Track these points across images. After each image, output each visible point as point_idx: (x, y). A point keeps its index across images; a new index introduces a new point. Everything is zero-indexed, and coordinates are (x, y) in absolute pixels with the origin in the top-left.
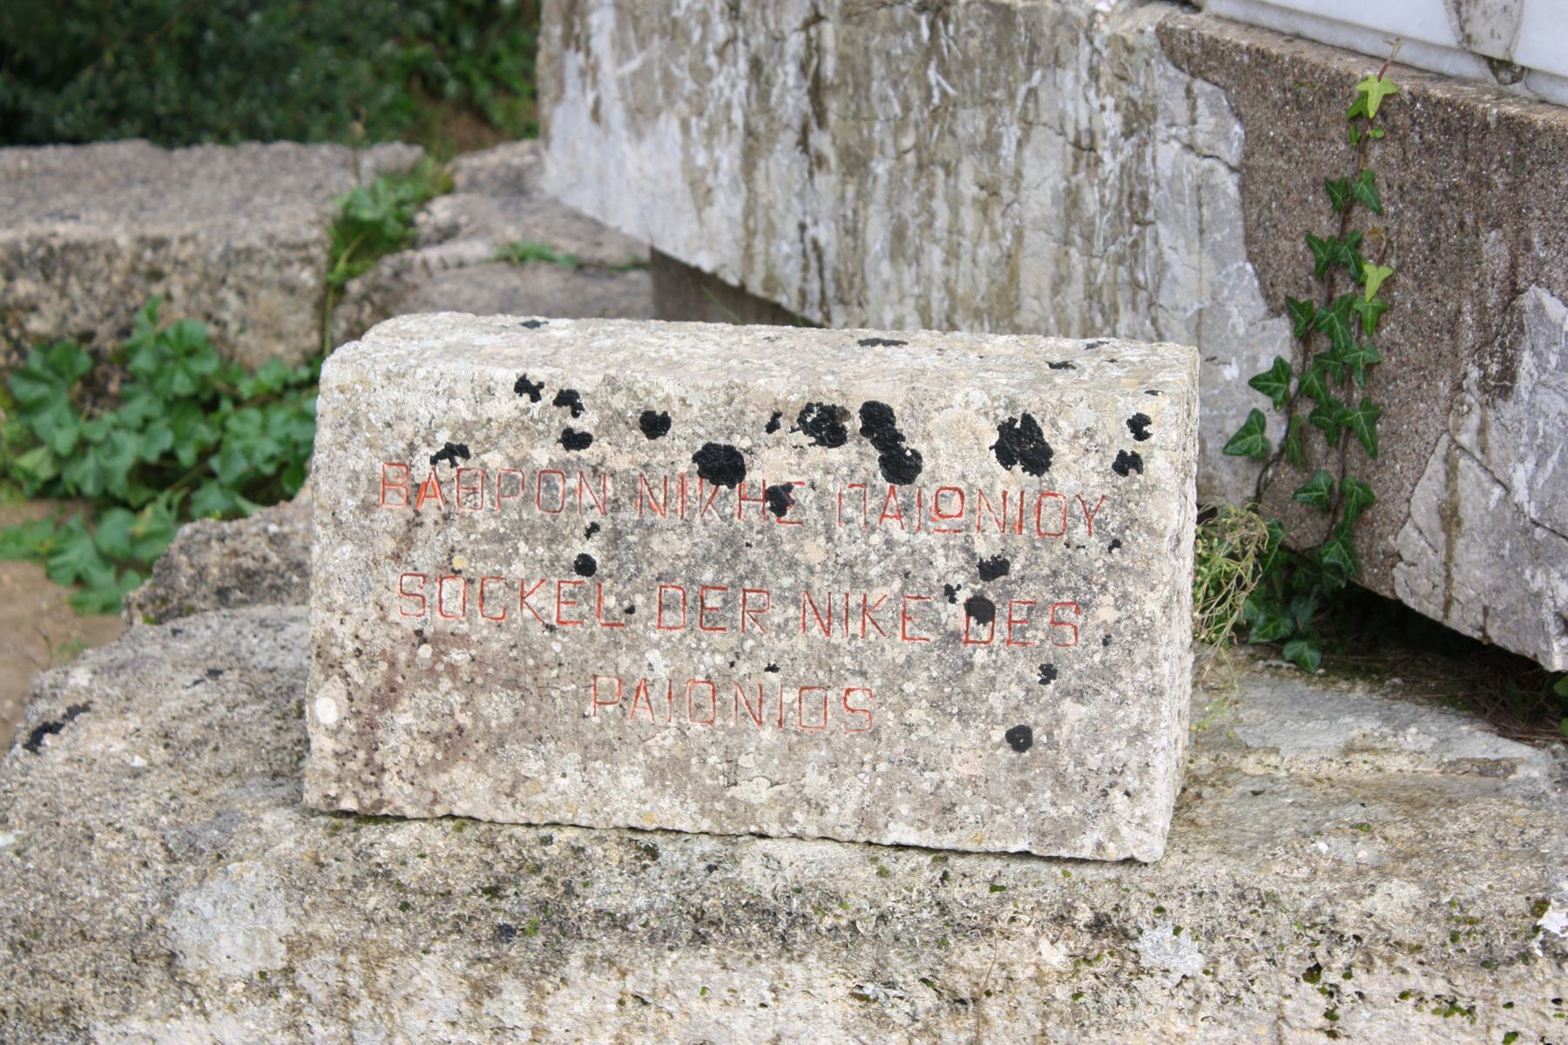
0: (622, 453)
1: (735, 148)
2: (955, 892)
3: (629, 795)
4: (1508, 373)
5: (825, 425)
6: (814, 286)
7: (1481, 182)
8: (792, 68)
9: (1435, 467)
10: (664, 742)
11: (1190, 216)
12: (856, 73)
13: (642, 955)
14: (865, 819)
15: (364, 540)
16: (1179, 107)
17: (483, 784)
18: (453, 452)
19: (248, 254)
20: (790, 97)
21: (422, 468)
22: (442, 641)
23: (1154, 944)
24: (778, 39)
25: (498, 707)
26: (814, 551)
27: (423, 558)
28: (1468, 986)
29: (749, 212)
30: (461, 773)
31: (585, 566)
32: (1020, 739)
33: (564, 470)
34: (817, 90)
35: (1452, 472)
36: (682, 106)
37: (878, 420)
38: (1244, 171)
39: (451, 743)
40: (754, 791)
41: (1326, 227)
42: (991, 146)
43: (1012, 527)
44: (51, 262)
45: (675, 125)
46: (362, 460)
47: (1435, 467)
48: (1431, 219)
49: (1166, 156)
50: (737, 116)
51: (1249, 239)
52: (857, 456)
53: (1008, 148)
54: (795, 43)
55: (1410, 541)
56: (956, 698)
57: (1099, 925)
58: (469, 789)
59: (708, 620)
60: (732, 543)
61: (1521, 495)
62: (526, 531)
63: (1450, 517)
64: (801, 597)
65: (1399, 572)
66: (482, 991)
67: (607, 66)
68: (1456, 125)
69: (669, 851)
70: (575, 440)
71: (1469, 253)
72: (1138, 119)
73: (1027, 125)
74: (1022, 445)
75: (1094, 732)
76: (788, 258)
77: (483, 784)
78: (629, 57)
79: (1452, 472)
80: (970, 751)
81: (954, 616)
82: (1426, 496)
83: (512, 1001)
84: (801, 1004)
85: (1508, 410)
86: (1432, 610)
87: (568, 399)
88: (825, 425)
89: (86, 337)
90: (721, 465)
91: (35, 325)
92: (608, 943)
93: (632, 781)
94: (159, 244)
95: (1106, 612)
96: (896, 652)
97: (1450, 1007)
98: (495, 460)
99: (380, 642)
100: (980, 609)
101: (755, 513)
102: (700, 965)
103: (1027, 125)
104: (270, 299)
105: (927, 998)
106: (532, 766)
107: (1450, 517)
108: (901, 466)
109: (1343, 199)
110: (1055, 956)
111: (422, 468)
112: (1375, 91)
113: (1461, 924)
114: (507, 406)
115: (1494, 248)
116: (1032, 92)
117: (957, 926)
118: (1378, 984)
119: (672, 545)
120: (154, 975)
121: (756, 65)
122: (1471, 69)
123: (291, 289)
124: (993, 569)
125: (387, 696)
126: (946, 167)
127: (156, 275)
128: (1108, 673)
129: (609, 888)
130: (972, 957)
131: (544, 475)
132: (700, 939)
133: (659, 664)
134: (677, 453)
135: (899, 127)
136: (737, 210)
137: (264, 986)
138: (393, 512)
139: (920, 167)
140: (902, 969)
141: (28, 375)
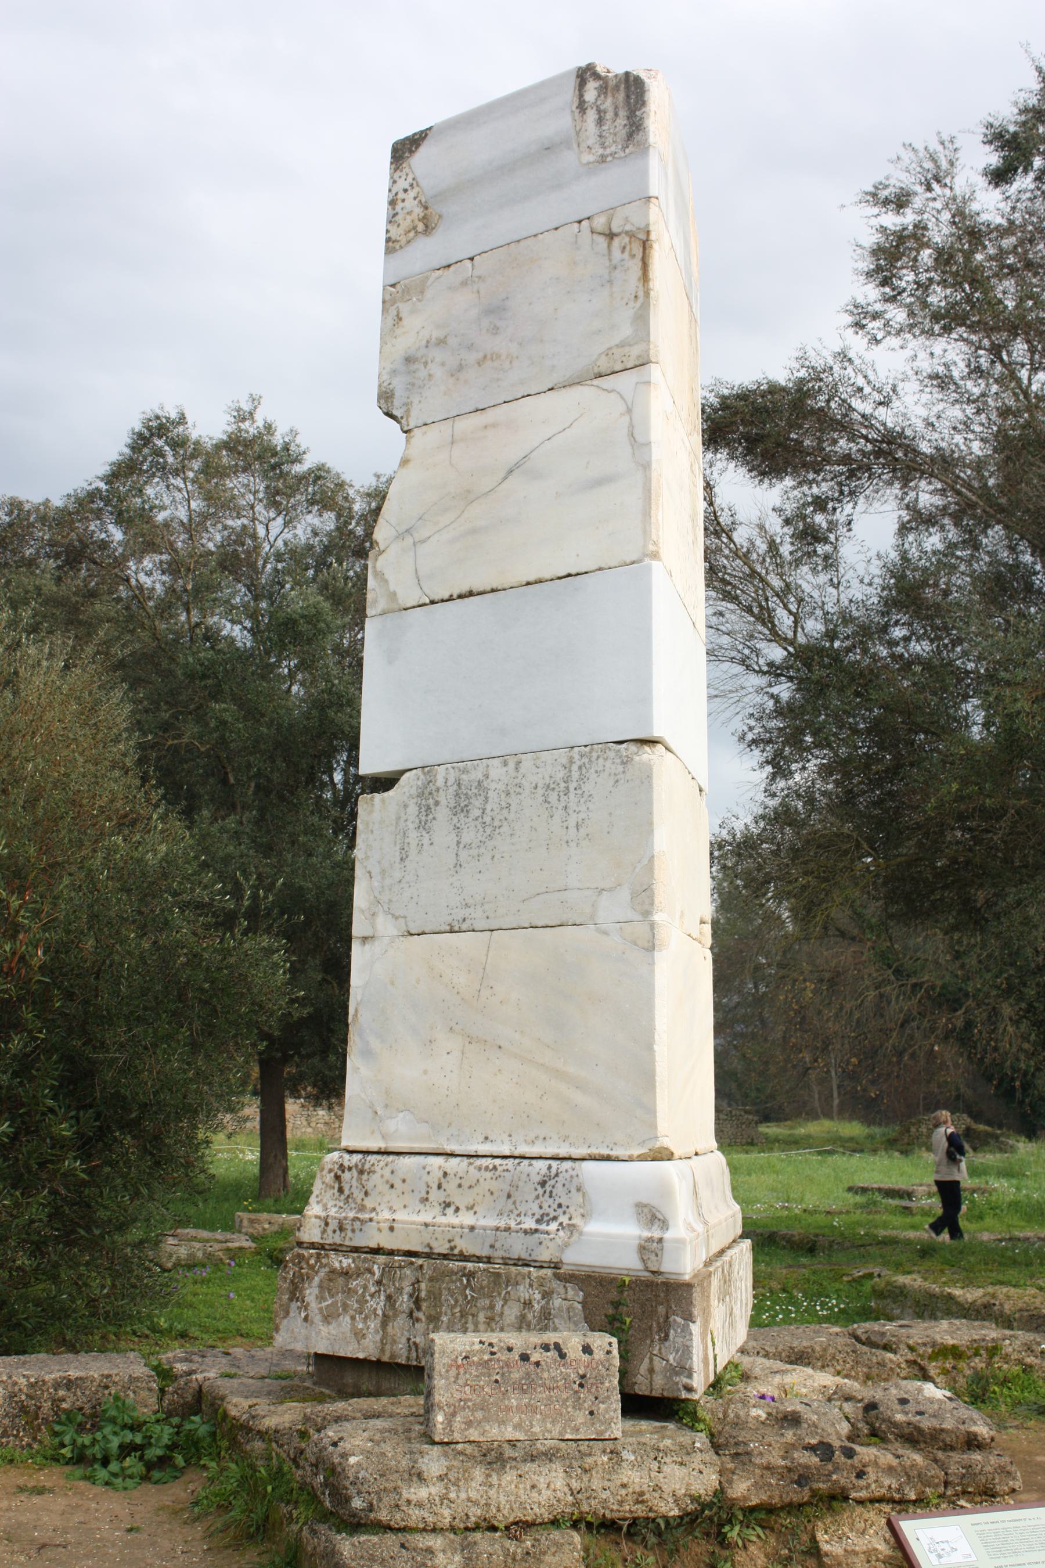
0: (503, 1356)
1: (378, 1321)
2: (581, 1448)
3: (510, 1433)
4: (667, 1335)
5: (546, 1347)
6: (414, 1355)
7: (656, 1296)
8: (406, 1297)
9: (647, 1360)
10: (516, 1420)
11: (565, 1316)
12: (435, 1297)
13: (521, 1465)
14: (560, 1433)
15: (447, 1379)
16: (562, 1290)
17: (476, 1433)
18: (466, 1357)
19: (137, 1379)
20: (404, 1302)
21: (460, 1361)
22: (466, 1400)
23: (625, 1455)
24: (400, 1290)
25: (479, 1415)
26: (546, 1375)
27: (461, 1382)
28: (686, 1458)
29: (383, 1337)
30: (471, 1431)
31: (497, 1381)
32: (591, 1413)
33: (490, 1360)
34: (417, 1302)
35: (651, 1360)
36: (352, 1312)
37: (557, 1346)
38: (584, 1303)
39: (469, 1424)
40: (536, 1429)
41: (611, 1312)
42: (492, 1307)
43: (586, 1367)
44: (69, 1384)
45: (348, 1319)
46: (446, 1360)
47: (647, 1360)
48: (643, 1305)
49: (557, 1302)
50: (380, 1312)
51: (586, 1318)
52: (553, 1354)
53: (498, 1307)
54: (408, 1289)
55: (639, 1379)
56: (578, 1405)
57: (612, 1452)
58: (474, 1435)
59: (524, 1391)
60: (528, 1374)
61: (671, 1361)
62: (482, 1374)
63: (651, 1371)
64: (544, 1385)
65: (636, 1387)
66: (488, 1476)
67: (314, 1305)
68: (649, 1285)
69: (519, 1444)
70: (493, 1353)
71: (654, 1311)
72: (547, 1295)
73: (505, 1301)
74: (587, 1349)
75: (607, 1411)
76: (987, 1183)
77: (476, 1433)
78: (325, 1300)
79: (651, 1360)
80: (581, 1417)
81: (576, 1387)
82: (643, 1368)
83: (494, 1479)
84: (554, 1474)
85: (667, 1344)
86: (647, 1393)
87: (491, 1345)
88: (546, 1347)
89: (81, 1409)
90: (525, 1357)
91: (64, 1405)
92: (514, 1463)
93: (510, 1429)
94: (109, 1376)
95: (607, 1384)
96: (564, 1396)
97: (681, 1464)
98: (475, 1359)
99: (452, 1401)
100: (581, 1385)
101: (532, 1367)
102: (534, 1466)
103: (505, 1301)
104: (144, 1394)
105: (579, 1471)
106: (487, 1428)
107: (651, 1371)
108: (563, 1356)
109: (616, 1305)
110: (605, 1459)
111: (460, 1361)
112: (627, 1279)
113: (682, 1446)
114: (477, 1347)
115: (662, 1310)
116: (508, 1293)
117: (583, 1455)
118: (668, 1460)
119: (516, 1375)
120: (415, 1479)
121: (389, 1298)
122: (647, 1274)
123: (150, 1390)
124: (583, 1377)
125: (454, 1414)
126: (473, 1315)
127: (107, 1387)
128: (608, 1397)
129: (508, 1452)
130: (590, 1460)
131: (487, 1362)
132: (533, 1461)
133: (514, 1402)
134: (515, 1356)
135: (453, 1307)
136: (378, 1338)
137: (441, 1478)
138: (453, 1372)
139: (462, 1316)
140: (575, 1464)
141: (59, 1423)
